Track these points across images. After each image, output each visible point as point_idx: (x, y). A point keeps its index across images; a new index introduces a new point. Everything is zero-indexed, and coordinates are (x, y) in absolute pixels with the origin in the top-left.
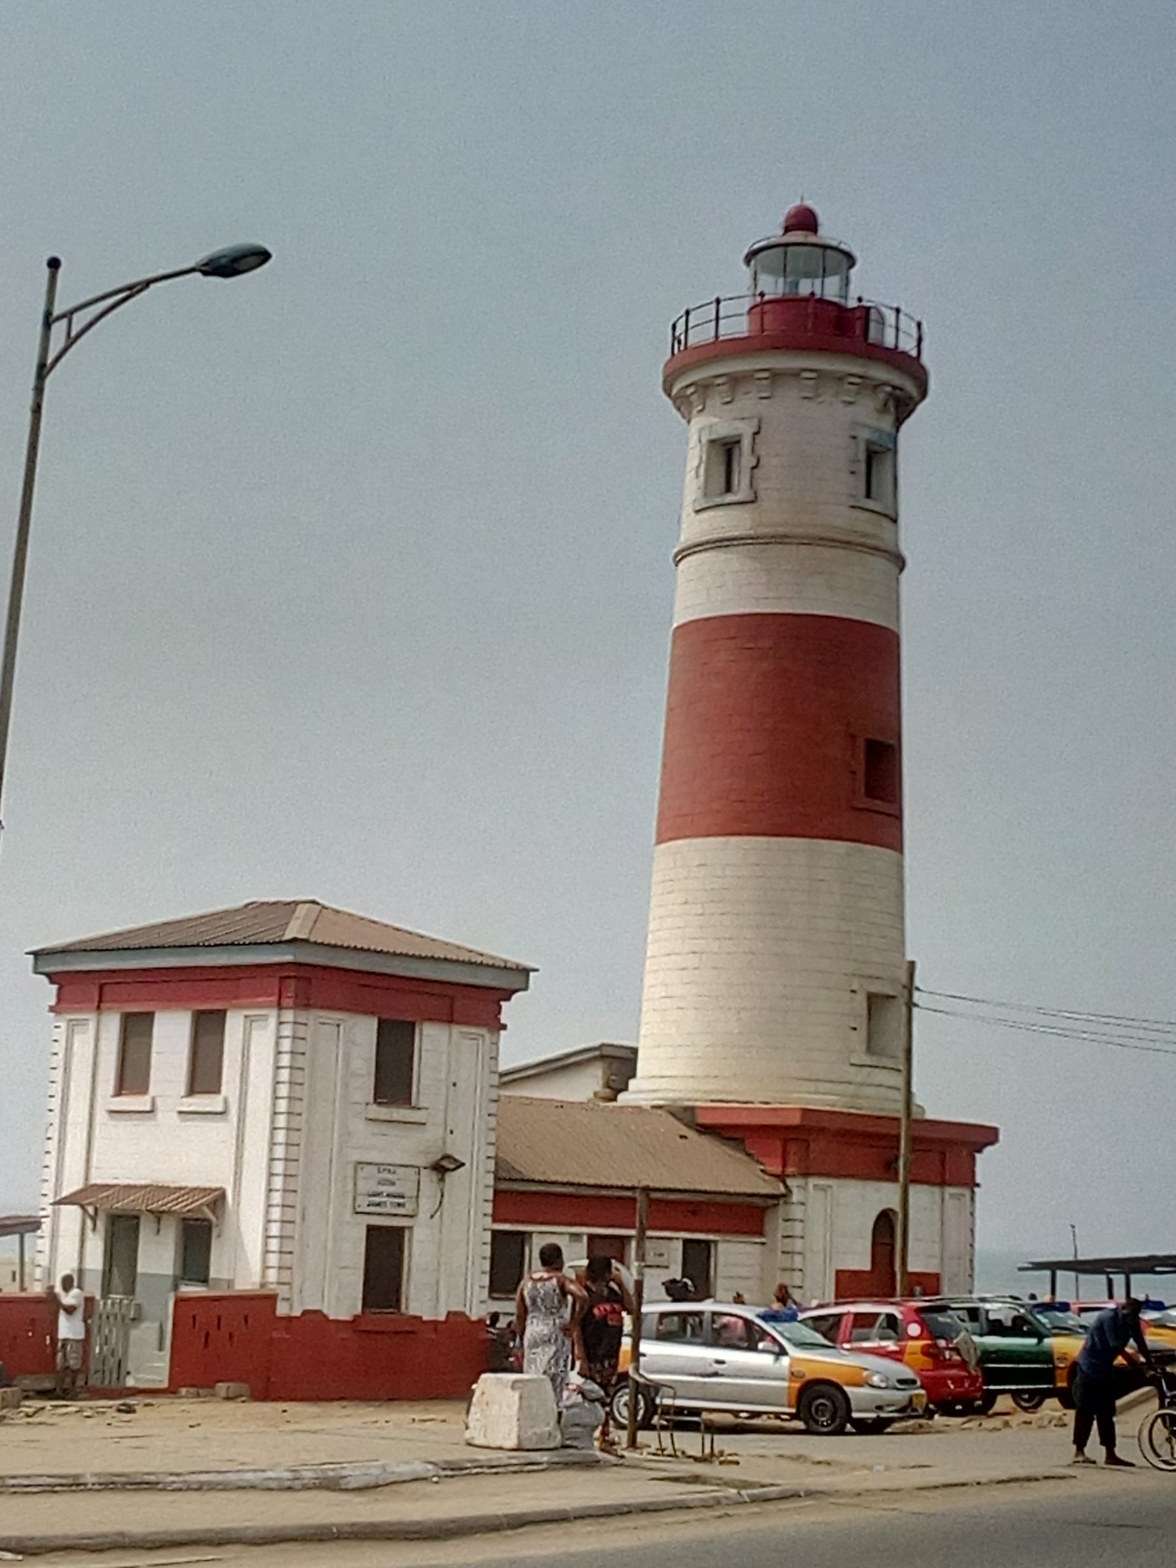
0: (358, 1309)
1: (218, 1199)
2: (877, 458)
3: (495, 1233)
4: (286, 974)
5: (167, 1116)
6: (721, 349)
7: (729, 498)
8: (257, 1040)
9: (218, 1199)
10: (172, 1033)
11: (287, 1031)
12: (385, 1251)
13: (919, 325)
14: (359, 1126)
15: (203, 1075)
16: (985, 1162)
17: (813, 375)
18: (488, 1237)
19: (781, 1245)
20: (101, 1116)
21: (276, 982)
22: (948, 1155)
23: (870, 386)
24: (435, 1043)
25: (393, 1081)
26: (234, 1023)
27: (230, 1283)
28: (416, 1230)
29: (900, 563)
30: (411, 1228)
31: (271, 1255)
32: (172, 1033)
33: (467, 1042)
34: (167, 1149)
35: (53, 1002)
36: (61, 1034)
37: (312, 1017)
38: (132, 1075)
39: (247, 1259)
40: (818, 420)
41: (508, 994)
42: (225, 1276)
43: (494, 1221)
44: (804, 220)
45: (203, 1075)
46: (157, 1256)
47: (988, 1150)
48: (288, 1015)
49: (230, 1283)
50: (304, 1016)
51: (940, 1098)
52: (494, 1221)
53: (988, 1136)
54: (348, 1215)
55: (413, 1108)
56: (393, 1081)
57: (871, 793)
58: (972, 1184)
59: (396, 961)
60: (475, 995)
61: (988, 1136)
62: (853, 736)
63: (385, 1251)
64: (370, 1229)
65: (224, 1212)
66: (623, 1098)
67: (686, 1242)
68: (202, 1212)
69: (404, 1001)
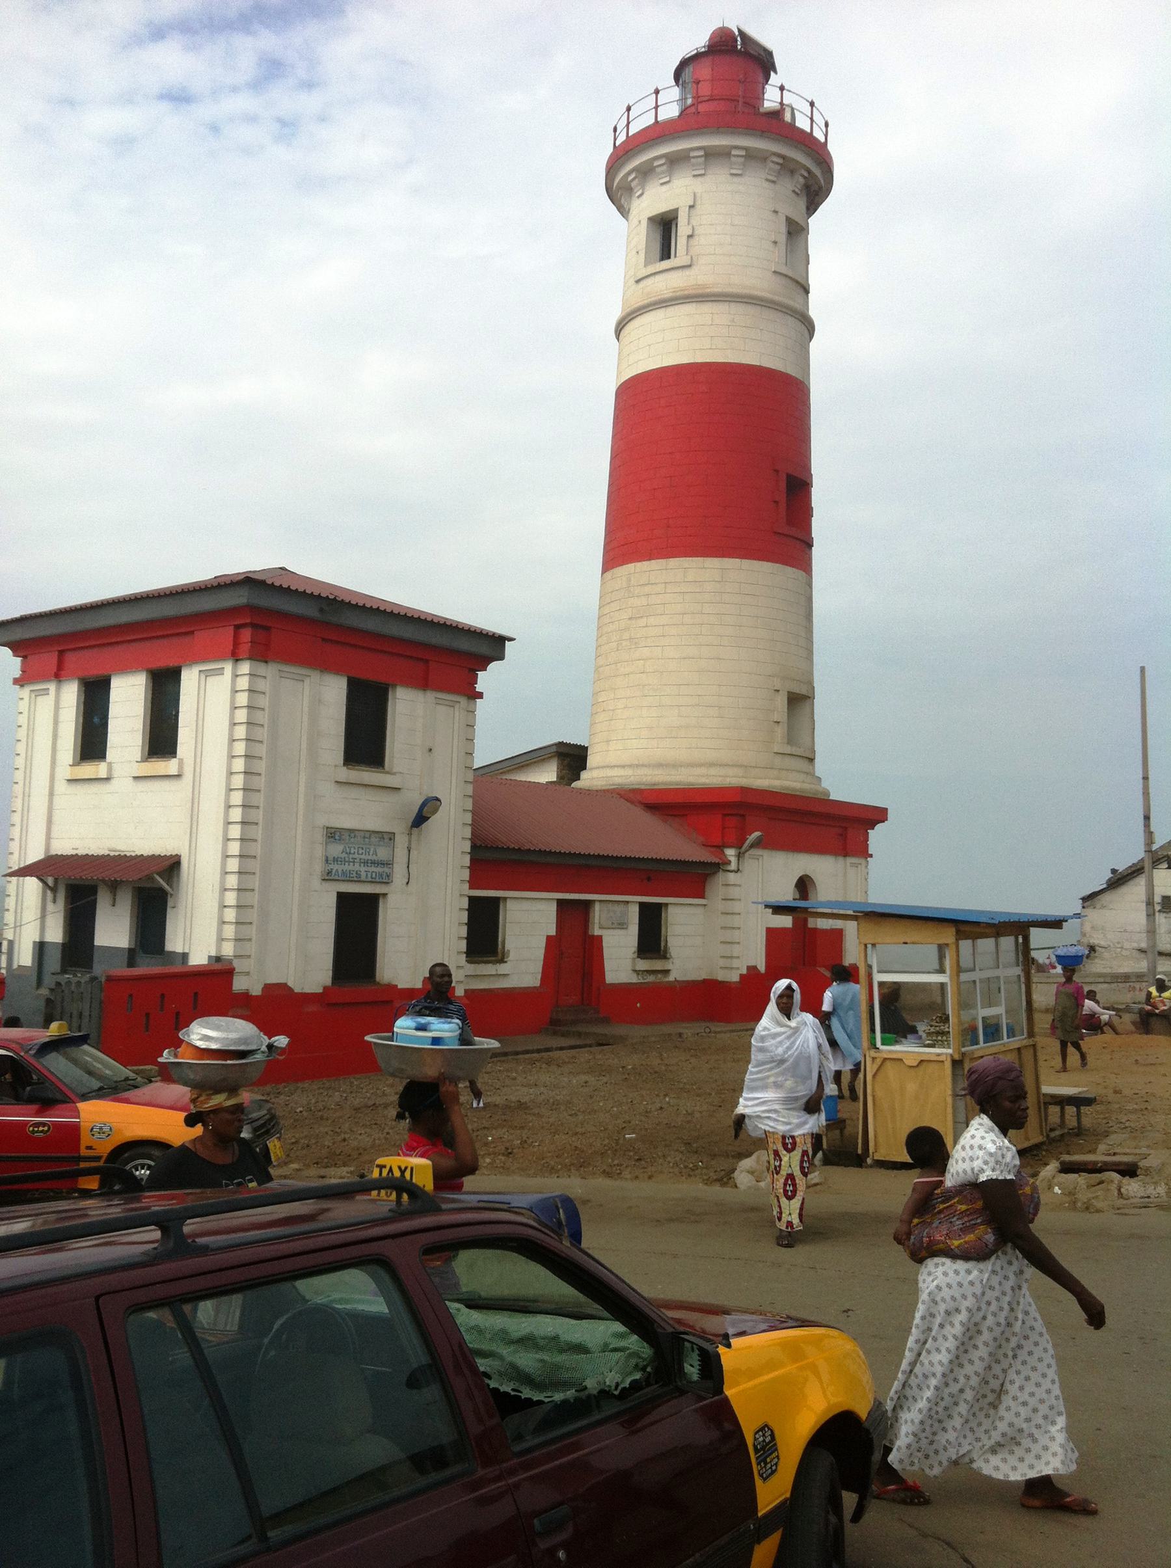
0: (328, 981)
1: (171, 866)
2: (796, 232)
3: (472, 900)
4: (242, 622)
5: (122, 784)
6: (658, 133)
7: (666, 264)
8: (213, 696)
9: (171, 866)
10: (128, 696)
11: (243, 683)
12: (357, 920)
13: (812, 104)
14: (327, 789)
15: (161, 739)
16: (877, 837)
17: (743, 153)
18: (465, 903)
19: (721, 906)
20: (61, 787)
21: (230, 630)
22: (845, 828)
23: (787, 167)
24: (409, 711)
25: (365, 742)
26: (190, 678)
27: (185, 956)
28: (391, 898)
29: (809, 327)
30: (385, 895)
31: (226, 927)
32: (128, 696)
33: (443, 708)
34: (120, 813)
35: (17, 673)
36: (23, 706)
37: (270, 670)
38: (92, 743)
39: (199, 933)
40: (722, 208)
41: (483, 662)
42: (179, 949)
43: (471, 888)
44: (729, 80)
45: (161, 739)
46: (113, 930)
47: (879, 827)
48: (245, 667)
49: (185, 956)
50: (262, 668)
51: (841, 779)
52: (471, 888)
53: (876, 816)
54: (316, 883)
55: (388, 773)
56: (365, 742)
57: (790, 522)
58: (864, 853)
59: (447, 1231)
60: (455, 656)
61: (876, 816)
62: (777, 471)
63: (357, 920)
64: (342, 897)
65: (178, 881)
66: (574, 785)
67: (641, 904)
68: (153, 879)
69: (377, 658)
